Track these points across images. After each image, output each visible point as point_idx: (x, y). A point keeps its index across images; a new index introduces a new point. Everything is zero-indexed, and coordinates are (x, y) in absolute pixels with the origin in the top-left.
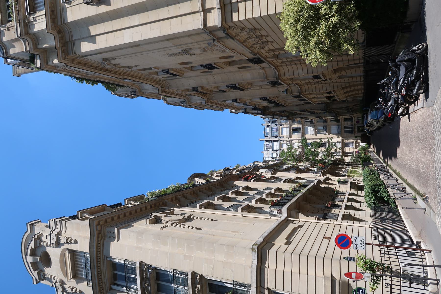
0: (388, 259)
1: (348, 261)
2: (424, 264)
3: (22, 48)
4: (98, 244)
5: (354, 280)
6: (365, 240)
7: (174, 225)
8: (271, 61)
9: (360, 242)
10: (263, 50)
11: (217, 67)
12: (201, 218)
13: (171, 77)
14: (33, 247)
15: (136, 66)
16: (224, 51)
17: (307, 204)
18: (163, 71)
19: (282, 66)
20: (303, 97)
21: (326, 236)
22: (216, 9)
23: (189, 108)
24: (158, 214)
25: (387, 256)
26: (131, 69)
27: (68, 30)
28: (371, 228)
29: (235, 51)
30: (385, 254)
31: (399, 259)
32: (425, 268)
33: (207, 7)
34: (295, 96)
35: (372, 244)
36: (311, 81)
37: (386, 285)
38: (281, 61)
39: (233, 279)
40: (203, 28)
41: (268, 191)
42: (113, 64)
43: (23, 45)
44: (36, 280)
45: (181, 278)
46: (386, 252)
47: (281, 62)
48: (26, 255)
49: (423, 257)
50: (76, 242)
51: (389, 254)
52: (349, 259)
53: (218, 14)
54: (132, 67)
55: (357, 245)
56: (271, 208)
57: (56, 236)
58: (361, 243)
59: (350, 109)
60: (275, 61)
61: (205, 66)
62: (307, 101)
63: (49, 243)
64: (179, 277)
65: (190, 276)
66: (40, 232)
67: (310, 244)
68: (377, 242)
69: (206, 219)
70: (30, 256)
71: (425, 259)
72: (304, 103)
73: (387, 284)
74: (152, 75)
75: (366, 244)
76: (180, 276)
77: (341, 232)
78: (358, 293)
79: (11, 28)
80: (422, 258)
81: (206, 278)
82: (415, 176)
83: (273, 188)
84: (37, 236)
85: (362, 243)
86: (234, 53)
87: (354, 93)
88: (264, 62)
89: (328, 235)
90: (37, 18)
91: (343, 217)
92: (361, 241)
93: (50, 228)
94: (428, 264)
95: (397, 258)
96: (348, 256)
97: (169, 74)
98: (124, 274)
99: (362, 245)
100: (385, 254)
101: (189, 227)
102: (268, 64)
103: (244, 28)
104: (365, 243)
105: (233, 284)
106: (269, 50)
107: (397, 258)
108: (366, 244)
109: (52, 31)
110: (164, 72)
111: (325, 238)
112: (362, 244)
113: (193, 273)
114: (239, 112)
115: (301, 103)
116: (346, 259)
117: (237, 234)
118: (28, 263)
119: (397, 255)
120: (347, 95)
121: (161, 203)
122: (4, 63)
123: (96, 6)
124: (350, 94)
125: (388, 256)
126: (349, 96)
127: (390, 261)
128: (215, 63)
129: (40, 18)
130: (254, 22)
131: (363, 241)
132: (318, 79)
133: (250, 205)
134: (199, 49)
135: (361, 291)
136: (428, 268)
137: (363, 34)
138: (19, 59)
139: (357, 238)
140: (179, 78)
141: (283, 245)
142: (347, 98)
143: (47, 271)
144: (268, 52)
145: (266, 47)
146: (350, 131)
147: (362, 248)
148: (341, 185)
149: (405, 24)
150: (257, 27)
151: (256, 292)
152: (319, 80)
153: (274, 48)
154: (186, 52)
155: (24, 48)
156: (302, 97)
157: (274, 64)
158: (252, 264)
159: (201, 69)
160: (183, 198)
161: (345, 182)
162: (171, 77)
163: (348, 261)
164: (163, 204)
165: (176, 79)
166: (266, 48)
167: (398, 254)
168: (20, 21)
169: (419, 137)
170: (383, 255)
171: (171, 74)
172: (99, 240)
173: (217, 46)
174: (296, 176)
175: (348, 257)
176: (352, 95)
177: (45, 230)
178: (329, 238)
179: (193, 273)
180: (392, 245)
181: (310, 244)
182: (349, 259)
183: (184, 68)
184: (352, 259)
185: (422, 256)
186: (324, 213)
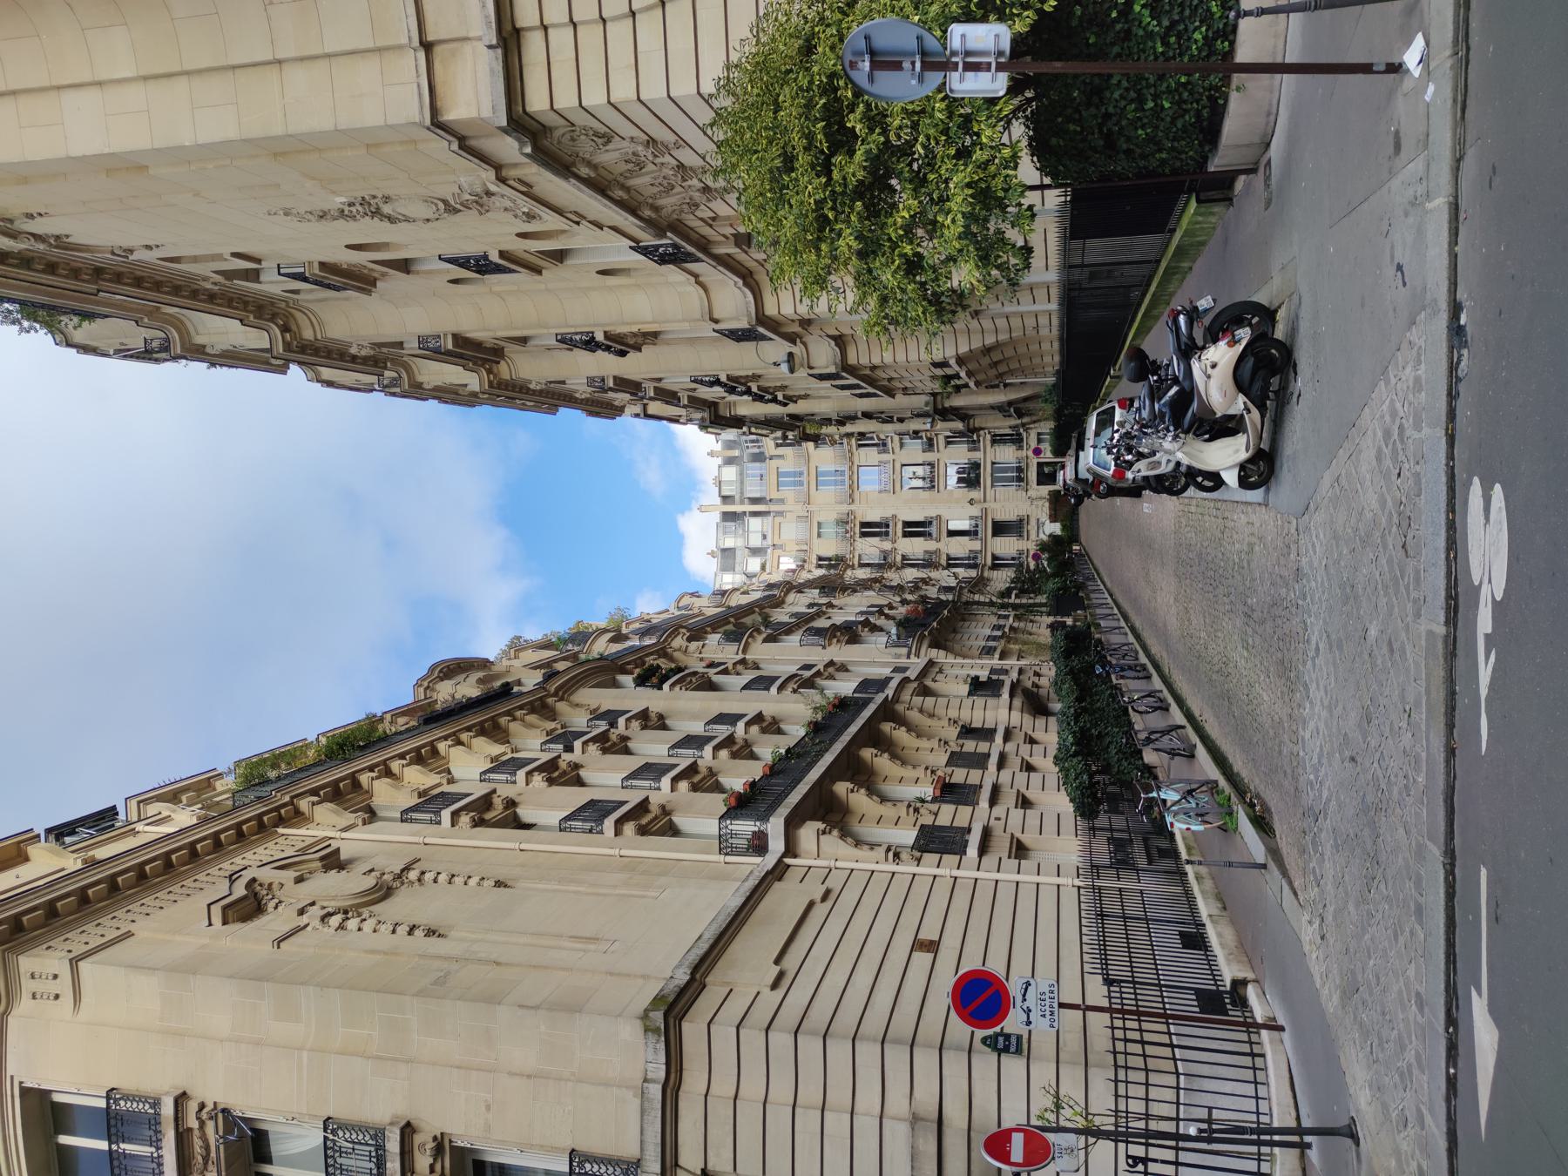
0: (1139, 1062)
1: (999, 1055)
6: (1056, 992)
7: (335, 921)
8: (727, 257)
9: (1039, 1002)
10: (692, 217)
15: (148, 247)
16: (530, 217)
18: (282, 271)
20: (848, 376)
22: (481, 48)
26: (127, 257)
28: (1079, 888)
29: (578, 219)
30: (1126, 1040)
31: (1174, 1037)
32: (1265, 1150)
34: (820, 375)
35: (1083, 1007)
37: (1130, 1161)
39: (569, 1144)
41: (722, 731)
42: (33, 235)
46: (1131, 1035)
49: (1256, 1049)
51: (1143, 1042)
53: (492, 71)
55: (1030, 1011)
56: (728, 822)
58: (1043, 1003)
60: (741, 257)
61: (461, 262)
62: (862, 388)
67: (863, 979)
68: (1097, 993)
71: (1263, 1056)
74: (235, 281)
75: (1061, 1005)
77: (971, 964)
80: (1252, 1055)
85: (1048, 1004)
88: (698, 260)
89: (928, 933)
92: (1043, 997)
94: (1276, 1124)
95: (1168, 1042)
98: (103, 1145)
99: (1048, 1013)
100: (1126, 1040)
101: (399, 929)
104: (1056, 1005)
108: (1061, 1005)
110: (284, 275)
111: (919, 945)
112: (1047, 1007)
116: (989, 1046)
117: (592, 947)
119: (1172, 1046)
125: (1137, 1048)
131: (1052, 995)
134: (426, 201)
137: (1063, 199)
139: (1028, 984)
141: (766, 991)
145: (703, 207)
146: (1011, 479)
147: (1046, 1021)
154: (372, 209)
157: (740, 266)
158: (645, 1080)
163: (999, 1055)
165: (346, 299)
170: (1120, 1046)
171: (316, 283)
173: (503, 196)
174: (827, 659)
178: (932, 942)
180: (1169, 1127)
181: (863, 979)
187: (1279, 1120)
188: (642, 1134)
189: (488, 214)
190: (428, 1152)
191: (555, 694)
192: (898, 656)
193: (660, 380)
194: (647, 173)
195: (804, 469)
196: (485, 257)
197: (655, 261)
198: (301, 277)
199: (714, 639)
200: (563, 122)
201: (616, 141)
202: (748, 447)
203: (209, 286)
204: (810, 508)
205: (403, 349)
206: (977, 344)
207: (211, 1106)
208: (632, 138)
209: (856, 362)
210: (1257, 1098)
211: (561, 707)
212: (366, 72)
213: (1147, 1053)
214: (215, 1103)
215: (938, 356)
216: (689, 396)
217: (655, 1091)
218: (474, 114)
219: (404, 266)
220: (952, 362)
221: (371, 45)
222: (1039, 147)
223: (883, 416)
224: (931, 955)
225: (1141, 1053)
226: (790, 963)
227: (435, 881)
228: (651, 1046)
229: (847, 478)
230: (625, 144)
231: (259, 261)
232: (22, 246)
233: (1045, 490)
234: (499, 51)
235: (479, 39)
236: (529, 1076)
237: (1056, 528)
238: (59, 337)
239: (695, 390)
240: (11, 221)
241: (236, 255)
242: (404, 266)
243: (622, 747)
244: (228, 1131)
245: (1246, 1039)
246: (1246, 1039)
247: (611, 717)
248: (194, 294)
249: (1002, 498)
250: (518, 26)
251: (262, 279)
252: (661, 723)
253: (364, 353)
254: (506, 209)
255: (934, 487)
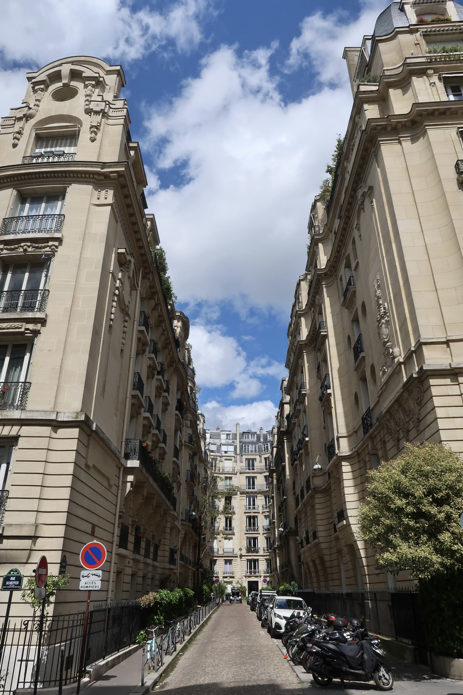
0: (66, 625)
2: (64, 682)
3: (388, 65)
4: (89, 174)
5: (37, 571)
10: (385, 433)
11: (358, 361)
12: (124, 332)
13: (342, 289)
14: (84, 75)
15: (360, 236)
17: (143, 499)
19: (359, 461)
21: (96, 528)
22: (450, 361)
23: (292, 315)
24: (132, 266)
25: (71, 625)
26: (356, 228)
27: (416, 134)
29: (383, 389)
30: (73, 621)
32: (58, 683)
33: (451, 344)
36: (335, 508)
37: (26, 622)
38: (367, 460)
39: (33, 382)
40: (421, 341)
42: (364, 201)
43: (392, 66)
44: (34, 78)
45: (36, 302)
46: (75, 622)
47: (365, 461)
48: (73, 63)
49: (68, 681)
50: (93, 140)
52: (64, 564)
53: (442, 365)
54: (359, 230)
57: (101, 109)
59: (286, 568)
62: (302, 500)
63: (90, 100)
64: (37, 298)
65: (39, 315)
66: (107, 85)
69: (123, 341)
70: (71, 69)
72: (298, 495)
73: (27, 624)
74: (345, 260)
76: (38, 299)
78: (14, 578)
79: (419, 49)
81: (36, 340)
82: (191, 670)
83: (166, 446)
84: (101, 81)
85: (91, 585)
86: (380, 388)
87: (313, 574)
88: (365, 433)
90: (434, 89)
91: (123, 556)
92: (94, 583)
93: (113, 100)
94: (64, 688)
96: (67, 563)
97: (347, 286)
99: (87, 585)
100: (73, 621)
102: (362, 440)
103: (420, 403)
105: (25, 382)
106: (384, 441)
107: (68, 639)
109: (415, 111)
111: (94, 526)
113: (43, 321)
114: (283, 392)
115: (298, 491)
118: (61, 65)
120: (311, 564)
121: (147, 271)
122: (364, 36)
123: (458, 184)
124: (312, 569)
126: (309, 568)
127: (57, 630)
128: (364, 357)
129: (435, 93)
130: (430, 418)
132: (337, 518)
133: (143, 410)
135: (17, 583)
136: (57, 688)
138: (372, 59)
140: (340, 301)
142: (305, 565)
143: (47, 97)
144: (381, 440)
145: (390, 437)
148: (167, 554)
149: (428, 653)
150: (422, 423)
151: (12, 418)
152: (336, 520)
153: (388, 449)
155: (389, 67)
156: (307, 493)
159: (354, 335)
160: (154, 305)
161: (172, 561)
162: (342, 289)
164: (147, 274)
165: (339, 297)
166: (387, 438)
167: (73, 640)
168: (429, 62)
169: (253, 675)
171: (347, 289)
172: (95, 176)
174: (181, 482)
175: (66, 562)
176: (310, 573)
177: (110, 94)
179: (43, 321)
182: (64, 564)
183: (357, 310)
184: (64, 570)
185: (70, 679)
186: (129, 526)
187: (40, 692)
188: (37, 411)
189: (383, 356)
190: (34, 328)
191: (176, 367)
192: (182, 513)
193: (305, 412)
194: (405, 418)
195: (255, 471)
196: (362, 351)
197: (363, 416)
198: (349, 283)
199: (190, 431)
200: (425, 389)
201: (418, 408)
202: (264, 445)
203: (343, 251)
204: (238, 474)
205: (318, 315)
206: (325, 552)
207: (56, 250)
208: (420, 414)
209: (316, 497)
210: (50, 681)
211: (172, 369)
212: (436, 320)
213: (64, 630)
214: (57, 251)
215: (320, 534)
216: (295, 423)
217: (53, 417)
218: (426, 357)
219: (356, 320)
220: (317, 541)
221: (445, 323)
222: (141, 598)
223: (284, 508)
224: (90, 533)
225: (64, 627)
226: (92, 472)
227: (124, 327)
228: (71, 415)
229: (252, 490)
230: (417, 410)
231: (355, 270)
232: (359, 197)
233: (246, 585)
234: (449, 368)
235: (452, 361)
236: (61, 367)
237: (229, 589)
238: (318, 198)
239: (299, 426)
240: (369, 196)
241: (358, 263)
242: (356, 320)
243: (158, 395)
244: (46, 255)
245: (57, 679)
246: (57, 679)
247: (167, 390)
248: (339, 246)
249: (242, 564)
250: (458, 375)
251: (346, 269)
252: (165, 410)
253: (317, 300)
254: (386, 363)
255: (247, 531)
